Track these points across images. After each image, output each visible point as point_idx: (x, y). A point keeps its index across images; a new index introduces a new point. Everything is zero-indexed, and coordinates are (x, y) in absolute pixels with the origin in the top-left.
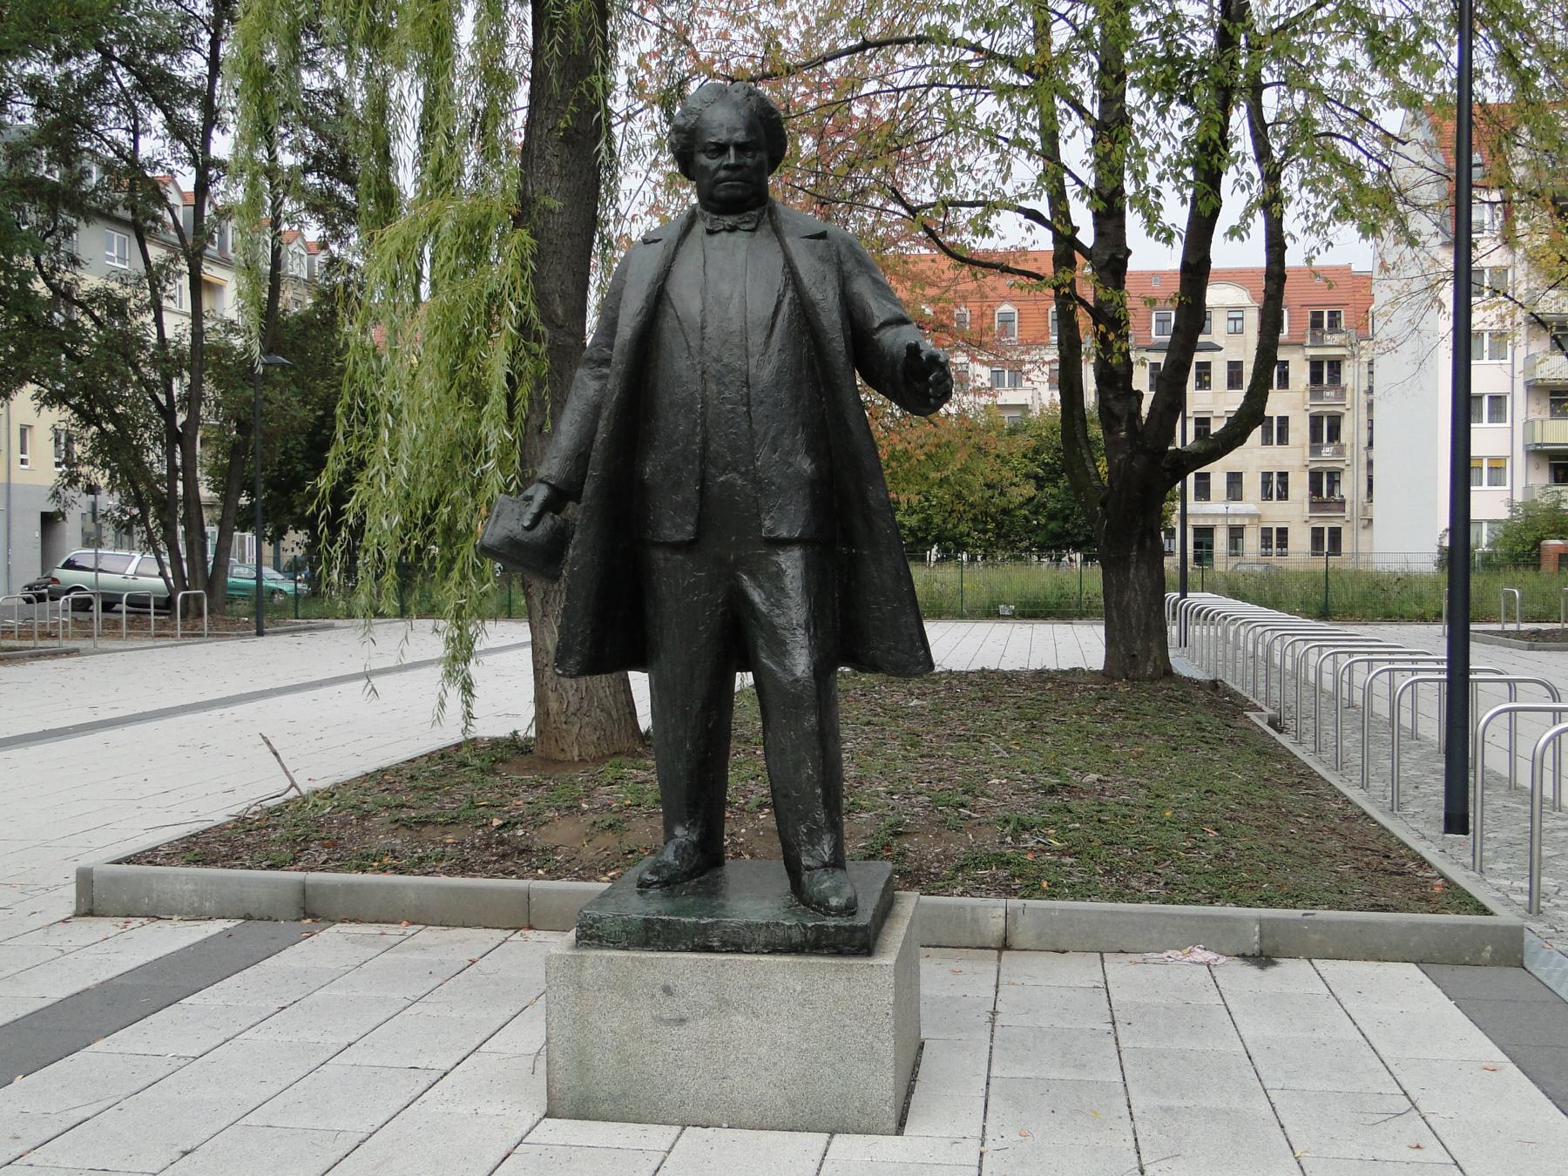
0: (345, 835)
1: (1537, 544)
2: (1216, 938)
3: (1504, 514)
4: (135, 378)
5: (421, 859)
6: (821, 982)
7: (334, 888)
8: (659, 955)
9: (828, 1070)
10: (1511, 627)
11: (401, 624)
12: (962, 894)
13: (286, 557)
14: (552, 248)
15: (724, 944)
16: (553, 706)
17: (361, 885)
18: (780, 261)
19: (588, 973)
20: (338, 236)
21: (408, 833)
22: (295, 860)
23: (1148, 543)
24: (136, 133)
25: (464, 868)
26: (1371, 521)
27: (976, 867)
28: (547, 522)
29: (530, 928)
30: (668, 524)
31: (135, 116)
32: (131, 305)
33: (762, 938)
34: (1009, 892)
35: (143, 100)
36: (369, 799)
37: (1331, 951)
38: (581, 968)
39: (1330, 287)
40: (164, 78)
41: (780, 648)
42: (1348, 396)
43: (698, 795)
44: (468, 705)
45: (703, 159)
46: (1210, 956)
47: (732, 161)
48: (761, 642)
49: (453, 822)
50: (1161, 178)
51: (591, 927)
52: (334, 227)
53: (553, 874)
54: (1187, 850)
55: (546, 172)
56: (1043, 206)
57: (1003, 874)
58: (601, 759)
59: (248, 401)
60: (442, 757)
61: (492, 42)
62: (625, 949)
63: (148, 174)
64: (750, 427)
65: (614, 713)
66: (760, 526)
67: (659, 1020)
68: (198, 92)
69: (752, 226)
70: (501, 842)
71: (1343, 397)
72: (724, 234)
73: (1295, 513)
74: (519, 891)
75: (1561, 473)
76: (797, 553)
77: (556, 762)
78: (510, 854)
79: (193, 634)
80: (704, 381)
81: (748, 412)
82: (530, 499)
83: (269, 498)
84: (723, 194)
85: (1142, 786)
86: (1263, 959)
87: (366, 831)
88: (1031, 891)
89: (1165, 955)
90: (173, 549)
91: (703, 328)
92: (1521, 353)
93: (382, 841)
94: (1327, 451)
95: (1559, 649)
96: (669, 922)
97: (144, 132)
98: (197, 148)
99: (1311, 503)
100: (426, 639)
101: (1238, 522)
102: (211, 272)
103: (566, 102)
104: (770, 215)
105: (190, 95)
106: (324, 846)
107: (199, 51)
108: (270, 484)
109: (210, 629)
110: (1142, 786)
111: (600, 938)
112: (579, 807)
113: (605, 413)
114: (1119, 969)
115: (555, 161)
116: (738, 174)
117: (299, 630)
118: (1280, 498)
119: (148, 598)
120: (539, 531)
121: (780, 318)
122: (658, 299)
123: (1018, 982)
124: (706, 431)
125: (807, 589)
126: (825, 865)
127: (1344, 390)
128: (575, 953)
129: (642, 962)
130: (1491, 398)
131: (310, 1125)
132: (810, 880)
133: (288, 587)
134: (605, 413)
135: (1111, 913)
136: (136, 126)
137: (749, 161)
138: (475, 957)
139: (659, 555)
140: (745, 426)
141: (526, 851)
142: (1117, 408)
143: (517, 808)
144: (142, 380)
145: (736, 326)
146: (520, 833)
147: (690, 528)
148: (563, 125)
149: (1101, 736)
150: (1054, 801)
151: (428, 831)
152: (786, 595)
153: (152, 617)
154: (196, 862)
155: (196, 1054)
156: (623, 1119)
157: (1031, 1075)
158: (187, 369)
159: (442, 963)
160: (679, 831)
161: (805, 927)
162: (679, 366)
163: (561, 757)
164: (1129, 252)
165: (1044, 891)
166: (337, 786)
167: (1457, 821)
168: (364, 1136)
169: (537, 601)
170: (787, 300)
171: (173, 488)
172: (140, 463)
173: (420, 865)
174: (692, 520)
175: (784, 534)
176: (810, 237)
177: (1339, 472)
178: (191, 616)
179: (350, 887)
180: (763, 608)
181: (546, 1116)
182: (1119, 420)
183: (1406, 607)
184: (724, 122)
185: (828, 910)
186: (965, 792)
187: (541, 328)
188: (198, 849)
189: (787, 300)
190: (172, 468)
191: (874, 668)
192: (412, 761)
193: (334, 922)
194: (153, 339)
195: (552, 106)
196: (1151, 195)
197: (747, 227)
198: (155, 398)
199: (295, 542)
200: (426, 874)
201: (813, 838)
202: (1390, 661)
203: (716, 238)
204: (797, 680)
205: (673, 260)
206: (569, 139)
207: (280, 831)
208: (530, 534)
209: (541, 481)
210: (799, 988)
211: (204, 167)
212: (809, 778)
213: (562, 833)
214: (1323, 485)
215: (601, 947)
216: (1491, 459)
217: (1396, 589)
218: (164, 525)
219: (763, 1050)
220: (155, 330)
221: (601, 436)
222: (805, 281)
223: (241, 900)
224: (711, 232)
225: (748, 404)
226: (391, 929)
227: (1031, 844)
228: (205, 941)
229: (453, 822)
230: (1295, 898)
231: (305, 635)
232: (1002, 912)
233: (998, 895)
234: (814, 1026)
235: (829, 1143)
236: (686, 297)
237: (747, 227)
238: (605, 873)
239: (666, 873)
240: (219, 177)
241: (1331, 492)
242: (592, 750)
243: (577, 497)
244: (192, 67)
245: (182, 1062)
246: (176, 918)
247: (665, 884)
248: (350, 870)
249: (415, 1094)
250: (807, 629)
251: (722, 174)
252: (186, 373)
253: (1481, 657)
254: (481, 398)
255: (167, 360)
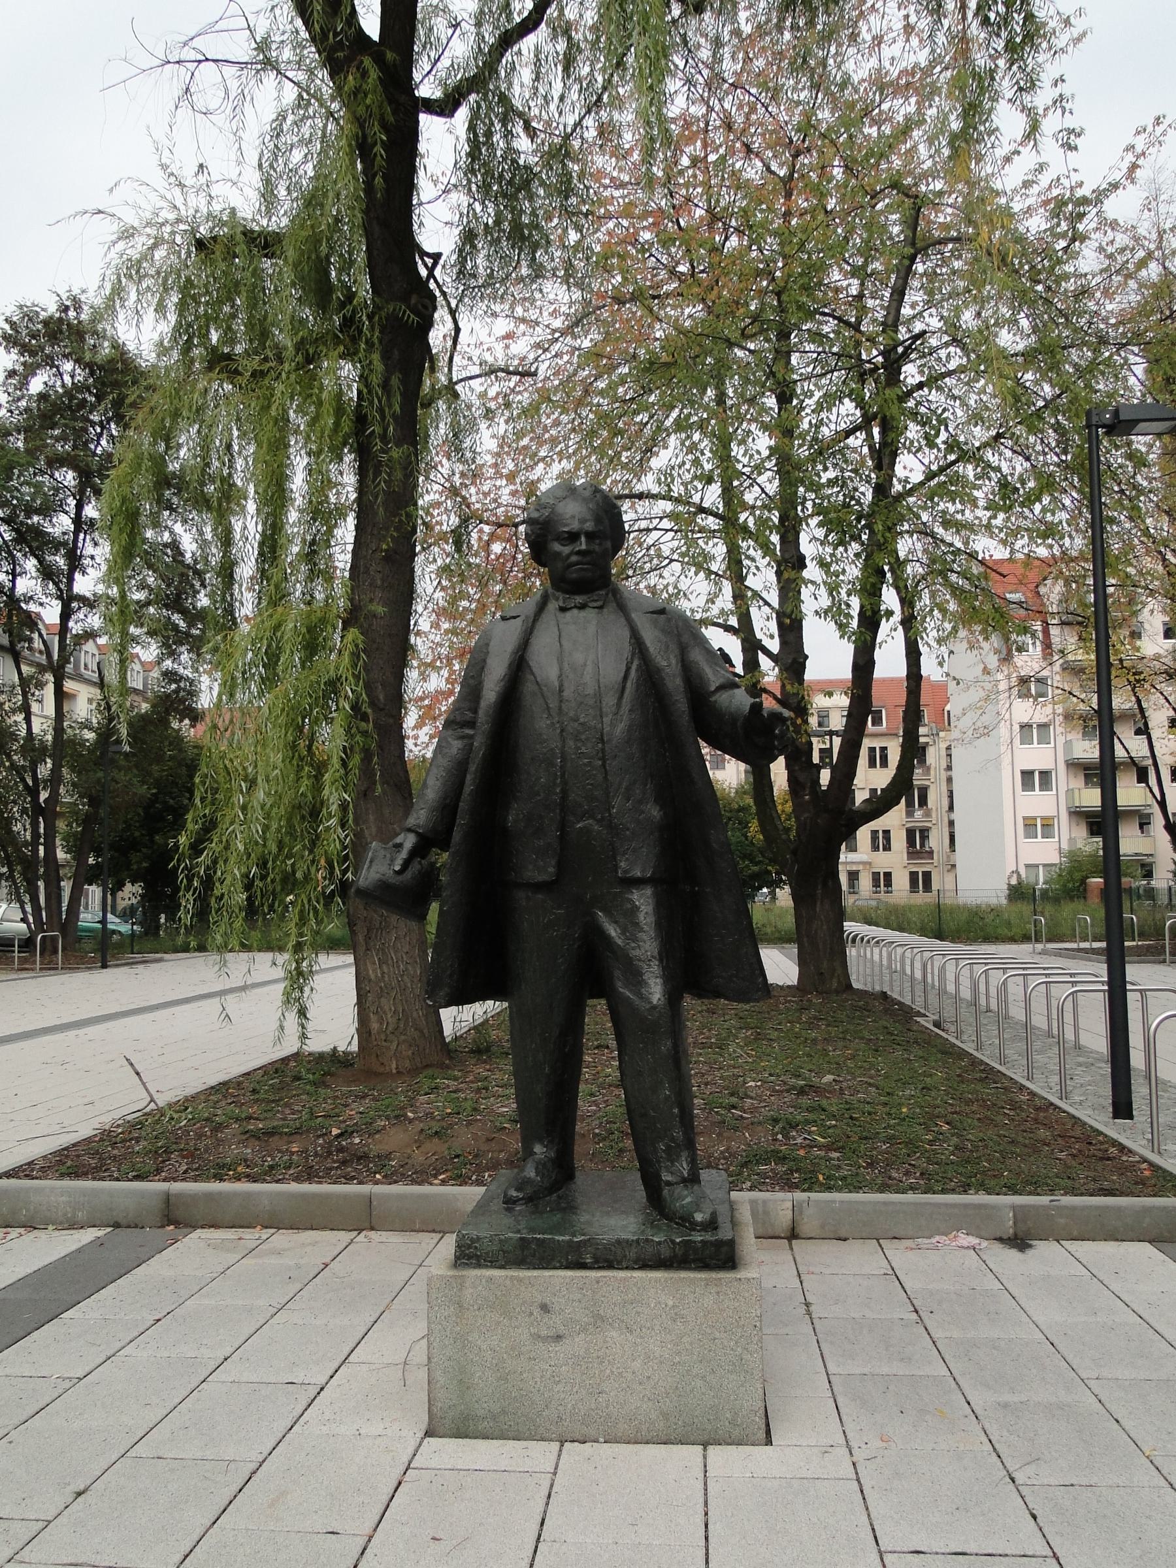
0: (202, 1146)
1: (1083, 882)
2: (976, 1223)
3: (1054, 859)
4: (7, 764)
5: (271, 1167)
6: (692, 1296)
7: (194, 1197)
8: (536, 1273)
9: (699, 1383)
10: (1074, 946)
11: (244, 956)
12: (751, 1189)
13: (122, 904)
14: (375, 646)
15: (597, 1262)
16: (375, 1026)
17: (220, 1193)
18: (626, 633)
19: (468, 1293)
20: (172, 654)
21: (257, 1143)
22: (158, 1171)
23: (830, 883)
24: (14, 575)
25: (309, 1175)
26: (954, 866)
27: (758, 1163)
28: (415, 867)
29: (372, 1229)
30: (531, 867)
31: (13, 561)
32: (6, 707)
33: (632, 1253)
34: (791, 1186)
35: (20, 551)
36: (219, 1112)
37: (1075, 1233)
38: (462, 1287)
39: (958, 683)
40: (38, 532)
41: (636, 978)
42: (932, 772)
43: (551, 1112)
44: (303, 1027)
45: (557, 547)
46: (973, 1241)
47: (584, 547)
48: (617, 973)
49: (297, 1132)
50: (849, 595)
51: (469, 1247)
52: (168, 646)
53: (390, 1179)
54: (931, 1143)
55: (371, 585)
56: (733, 621)
57: (782, 1169)
58: (414, 1071)
59: (99, 780)
60: (276, 1071)
61: (321, 484)
62: (502, 1267)
63: (23, 605)
64: (606, 778)
65: (425, 1031)
66: (616, 867)
67: (537, 1337)
68: (64, 544)
69: (599, 604)
70: (341, 1150)
71: (929, 774)
72: (575, 611)
73: (896, 861)
74: (359, 1196)
75: (1095, 828)
76: (649, 891)
77: (377, 1074)
78: (351, 1162)
79: (50, 967)
80: (564, 741)
81: (604, 765)
82: (399, 846)
83: (112, 858)
84: (574, 575)
85: (870, 1085)
86: (1019, 1241)
87: (220, 1142)
88: (809, 1184)
89: (934, 1240)
90: (34, 900)
91: (561, 691)
92: (1061, 740)
93: (235, 1150)
94: (918, 814)
95: (1154, 962)
96: (544, 1240)
97: (20, 575)
98: (62, 586)
99: (908, 853)
100: (268, 968)
101: (854, 868)
102: (69, 685)
103: (387, 529)
104: (614, 595)
105: (57, 545)
106: (184, 1157)
107: (66, 513)
108: (112, 847)
109: (63, 963)
110: (870, 1085)
111: (478, 1257)
112: (405, 1115)
113: (472, 768)
114: (899, 1254)
115: (379, 576)
116: (588, 559)
117: (137, 963)
118: (884, 850)
119: (13, 940)
120: (408, 875)
121: (629, 684)
122: (519, 666)
123: (817, 1270)
124: (565, 783)
125: (658, 925)
126: (684, 1181)
127: (929, 768)
128: (451, 1273)
129: (520, 1280)
130: (1041, 773)
131: (199, 1455)
132: (671, 1196)
133: (125, 928)
134: (472, 768)
135: (885, 1203)
136: (14, 570)
137: (597, 548)
138: (327, 1260)
139: (521, 896)
140: (600, 777)
141: (363, 1158)
142: (802, 777)
143: (351, 1118)
144: (13, 766)
145: (590, 691)
146: (357, 1141)
147: (551, 870)
148: (384, 547)
149: (814, 1041)
150: (805, 1101)
151: (275, 1141)
152: (638, 931)
153: (16, 954)
154: (69, 1175)
155: (80, 1374)
156: (503, 1436)
157: (866, 1371)
158: (50, 757)
159: (298, 1266)
160: (538, 1149)
161: (673, 1242)
162: (539, 724)
163: (381, 1070)
164: (807, 657)
165: (822, 1184)
166: (186, 1099)
167: (1122, 1108)
168: (254, 1466)
169: (361, 938)
170: (634, 667)
171: (35, 851)
172: (10, 831)
173: (269, 1174)
174: (553, 862)
175: (638, 873)
176: (652, 612)
177: (928, 829)
178: (47, 953)
179: (209, 1196)
180: (619, 942)
181: (429, 1433)
182: (803, 787)
183: (999, 931)
184: (573, 514)
185: (694, 1226)
186: (732, 1095)
187: (369, 711)
188: (71, 1162)
189: (634, 667)
190: (36, 834)
191: (717, 995)
192: (248, 1074)
193: (195, 1227)
194: (23, 733)
195: (375, 532)
196: (843, 607)
197: (595, 604)
198: (23, 780)
199: (130, 893)
200: (277, 1181)
201: (672, 1155)
202: (1047, 975)
203: (568, 614)
204: (654, 1007)
205: (531, 633)
206: (388, 558)
207: (143, 1143)
208: (400, 878)
209: (410, 830)
210: (671, 1303)
211: (69, 603)
212: (667, 1098)
213: (394, 1140)
214: (916, 840)
215: (479, 1266)
216: (1042, 818)
217: (991, 917)
218: (26, 879)
219: (637, 1364)
220: (25, 726)
221: (469, 787)
222: (651, 650)
223: (111, 1209)
224: (563, 609)
225: (603, 759)
226: (247, 1234)
227: (799, 1141)
228: (79, 1251)
229: (297, 1132)
230: (1034, 1185)
231: (141, 967)
232: (790, 1205)
233: (782, 1189)
234: (685, 1340)
235: (705, 1457)
236: (545, 663)
237: (595, 604)
238: (436, 1178)
239: (529, 1190)
240: (80, 608)
241: (922, 845)
242: (407, 1064)
243: (445, 846)
244: (62, 524)
245: (67, 1384)
246: (51, 1227)
247: (529, 1200)
248: (207, 1180)
249: (296, 1414)
250: (661, 960)
251: (574, 558)
252: (48, 760)
253: (1135, 973)
254: (320, 768)
255: (33, 750)
